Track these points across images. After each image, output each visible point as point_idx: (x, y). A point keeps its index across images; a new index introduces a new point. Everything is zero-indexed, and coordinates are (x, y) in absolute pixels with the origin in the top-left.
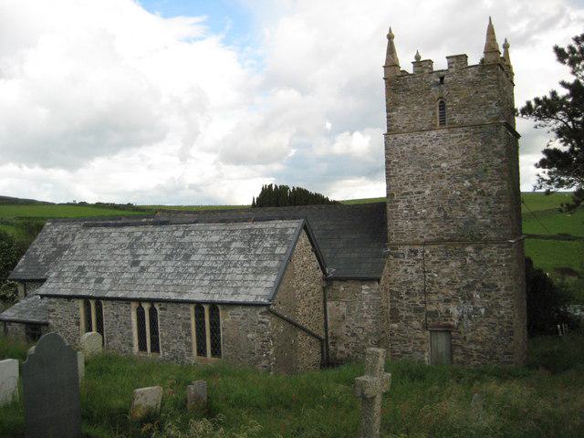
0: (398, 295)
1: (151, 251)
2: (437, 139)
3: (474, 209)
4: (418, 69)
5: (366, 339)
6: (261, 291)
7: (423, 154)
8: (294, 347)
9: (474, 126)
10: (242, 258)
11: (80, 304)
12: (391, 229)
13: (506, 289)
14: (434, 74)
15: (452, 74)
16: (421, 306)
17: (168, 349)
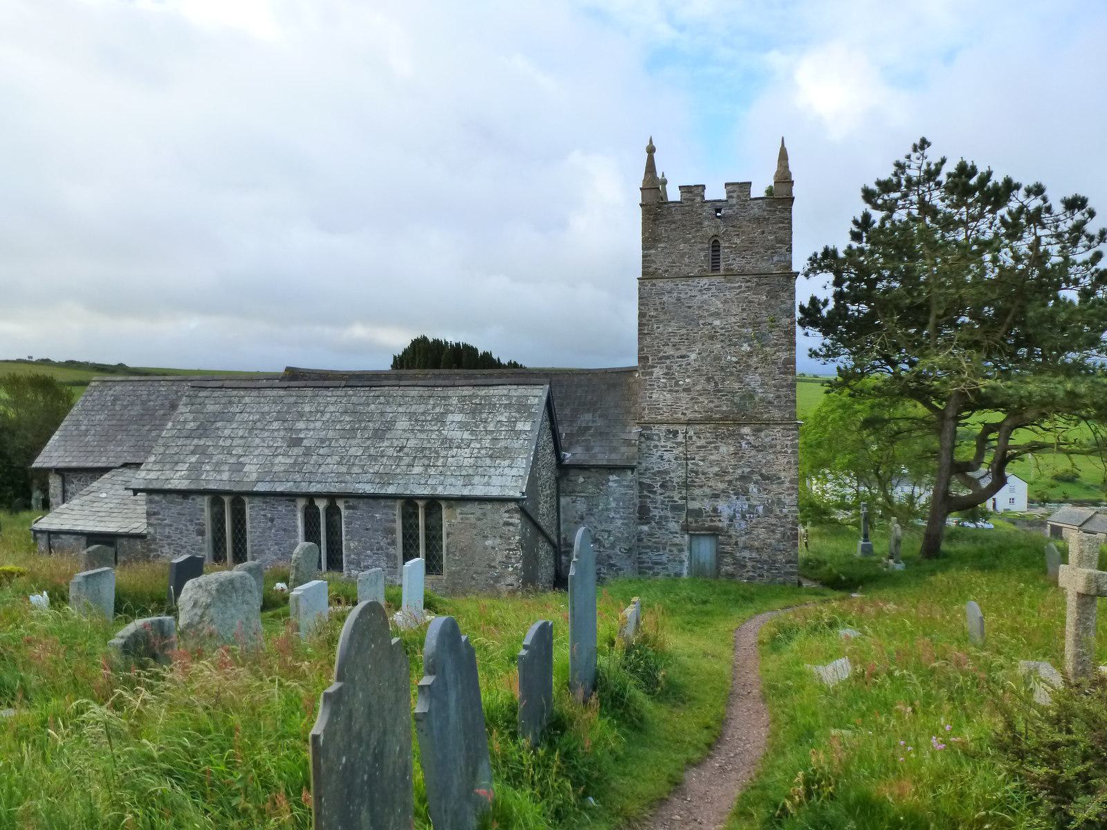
0: (650, 488)
1: (318, 424)
2: (709, 289)
5: (613, 546)
7: (689, 307)
9: (759, 275)
10: (466, 435)
11: (205, 502)
13: (791, 482)
15: (731, 206)
16: (680, 502)
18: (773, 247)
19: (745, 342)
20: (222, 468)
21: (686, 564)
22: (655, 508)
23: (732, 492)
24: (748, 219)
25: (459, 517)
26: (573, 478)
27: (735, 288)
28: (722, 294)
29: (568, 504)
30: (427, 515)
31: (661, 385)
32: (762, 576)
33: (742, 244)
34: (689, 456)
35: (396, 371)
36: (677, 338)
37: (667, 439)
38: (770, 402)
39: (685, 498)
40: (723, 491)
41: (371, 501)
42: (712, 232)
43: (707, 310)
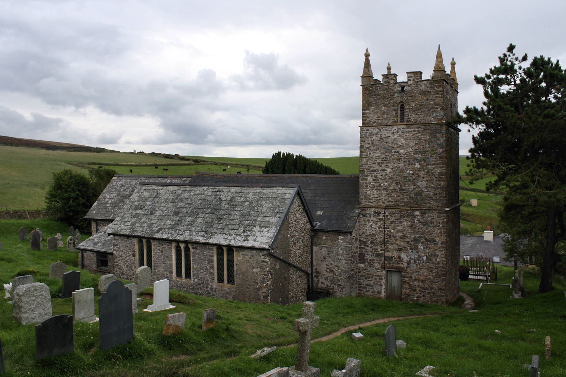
2: (397, 132)
3: (422, 184)
4: (386, 80)
5: (340, 275)
6: (264, 240)
7: (387, 142)
8: (287, 279)
9: (425, 124)
11: (135, 241)
12: (362, 196)
14: (397, 85)
16: (381, 252)
17: (197, 276)
18: (433, 108)
19: (417, 163)
20: (144, 225)
21: (384, 287)
22: (368, 254)
23: (409, 248)
24: (418, 92)
25: (242, 256)
26: (320, 237)
27: (411, 131)
28: (404, 135)
29: (318, 250)
30: (228, 255)
31: (371, 186)
32: (425, 296)
33: (416, 107)
34: (386, 227)
35: (265, 175)
36: (380, 160)
37: (374, 217)
38: (431, 197)
39: (384, 250)
40: (404, 247)
41: (203, 246)
42: (400, 100)
43: (397, 144)
